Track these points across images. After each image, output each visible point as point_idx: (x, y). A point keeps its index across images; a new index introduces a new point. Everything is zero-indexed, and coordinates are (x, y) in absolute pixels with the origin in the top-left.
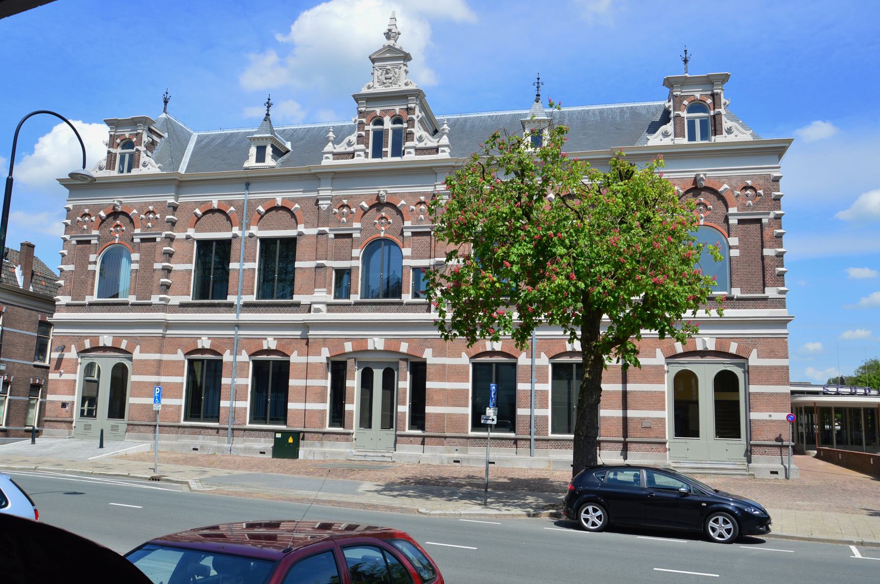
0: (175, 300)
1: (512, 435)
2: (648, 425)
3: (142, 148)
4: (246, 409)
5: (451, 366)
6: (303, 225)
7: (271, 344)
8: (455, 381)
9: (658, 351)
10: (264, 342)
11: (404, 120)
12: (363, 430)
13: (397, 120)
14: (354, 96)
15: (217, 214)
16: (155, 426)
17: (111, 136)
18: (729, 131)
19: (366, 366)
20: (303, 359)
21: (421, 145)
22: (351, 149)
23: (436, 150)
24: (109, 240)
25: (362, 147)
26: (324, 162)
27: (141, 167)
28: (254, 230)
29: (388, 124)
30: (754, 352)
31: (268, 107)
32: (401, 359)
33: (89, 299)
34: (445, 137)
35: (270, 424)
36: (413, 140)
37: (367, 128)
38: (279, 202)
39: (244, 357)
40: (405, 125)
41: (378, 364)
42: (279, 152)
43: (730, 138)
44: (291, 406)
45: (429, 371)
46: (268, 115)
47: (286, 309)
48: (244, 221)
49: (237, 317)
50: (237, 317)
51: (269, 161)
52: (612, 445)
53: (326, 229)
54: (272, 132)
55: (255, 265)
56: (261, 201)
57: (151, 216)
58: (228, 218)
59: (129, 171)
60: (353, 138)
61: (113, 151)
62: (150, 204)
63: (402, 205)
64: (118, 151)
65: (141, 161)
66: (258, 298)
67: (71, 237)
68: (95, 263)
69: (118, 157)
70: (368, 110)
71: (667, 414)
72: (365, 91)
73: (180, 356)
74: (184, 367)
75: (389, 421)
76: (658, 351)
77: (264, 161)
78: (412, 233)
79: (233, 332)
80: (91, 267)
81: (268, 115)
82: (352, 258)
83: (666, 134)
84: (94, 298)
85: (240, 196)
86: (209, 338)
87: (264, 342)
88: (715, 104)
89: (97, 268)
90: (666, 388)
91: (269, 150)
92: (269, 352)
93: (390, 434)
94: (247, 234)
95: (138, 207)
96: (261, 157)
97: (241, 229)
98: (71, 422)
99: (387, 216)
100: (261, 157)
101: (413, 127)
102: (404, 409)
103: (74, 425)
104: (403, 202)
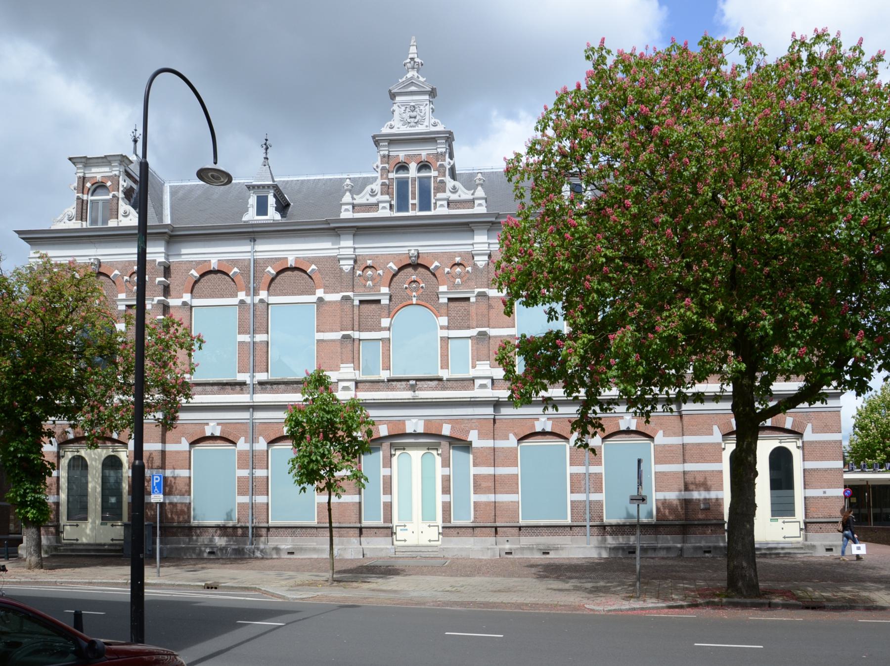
9: (715, 428)
10: (621, 422)
13: (424, 166)
15: (296, 272)
21: (454, 197)
22: (373, 200)
23: (471, 203)
25: (387, 198)
29: (413, 172)
30: (809, 427)
31: (267, 149)
34: (480, 188)
36: (445, 191)
40: (434, 173)
42: (283, 207)
49: (252, 398)
53: (350, 294)
54: (274, 181)
56: (393, 257)
61: (85, 197)
63: (116, 275)
65: (121, 212)
76: (715, 428)
77: (266, 214)
82: (382, 329)
86: (218, 424)
87: (536, 423)
91: (272, 201)
94: (257, 299)
95: (120, 267)
96: (262, 209)
100: (262, 209)
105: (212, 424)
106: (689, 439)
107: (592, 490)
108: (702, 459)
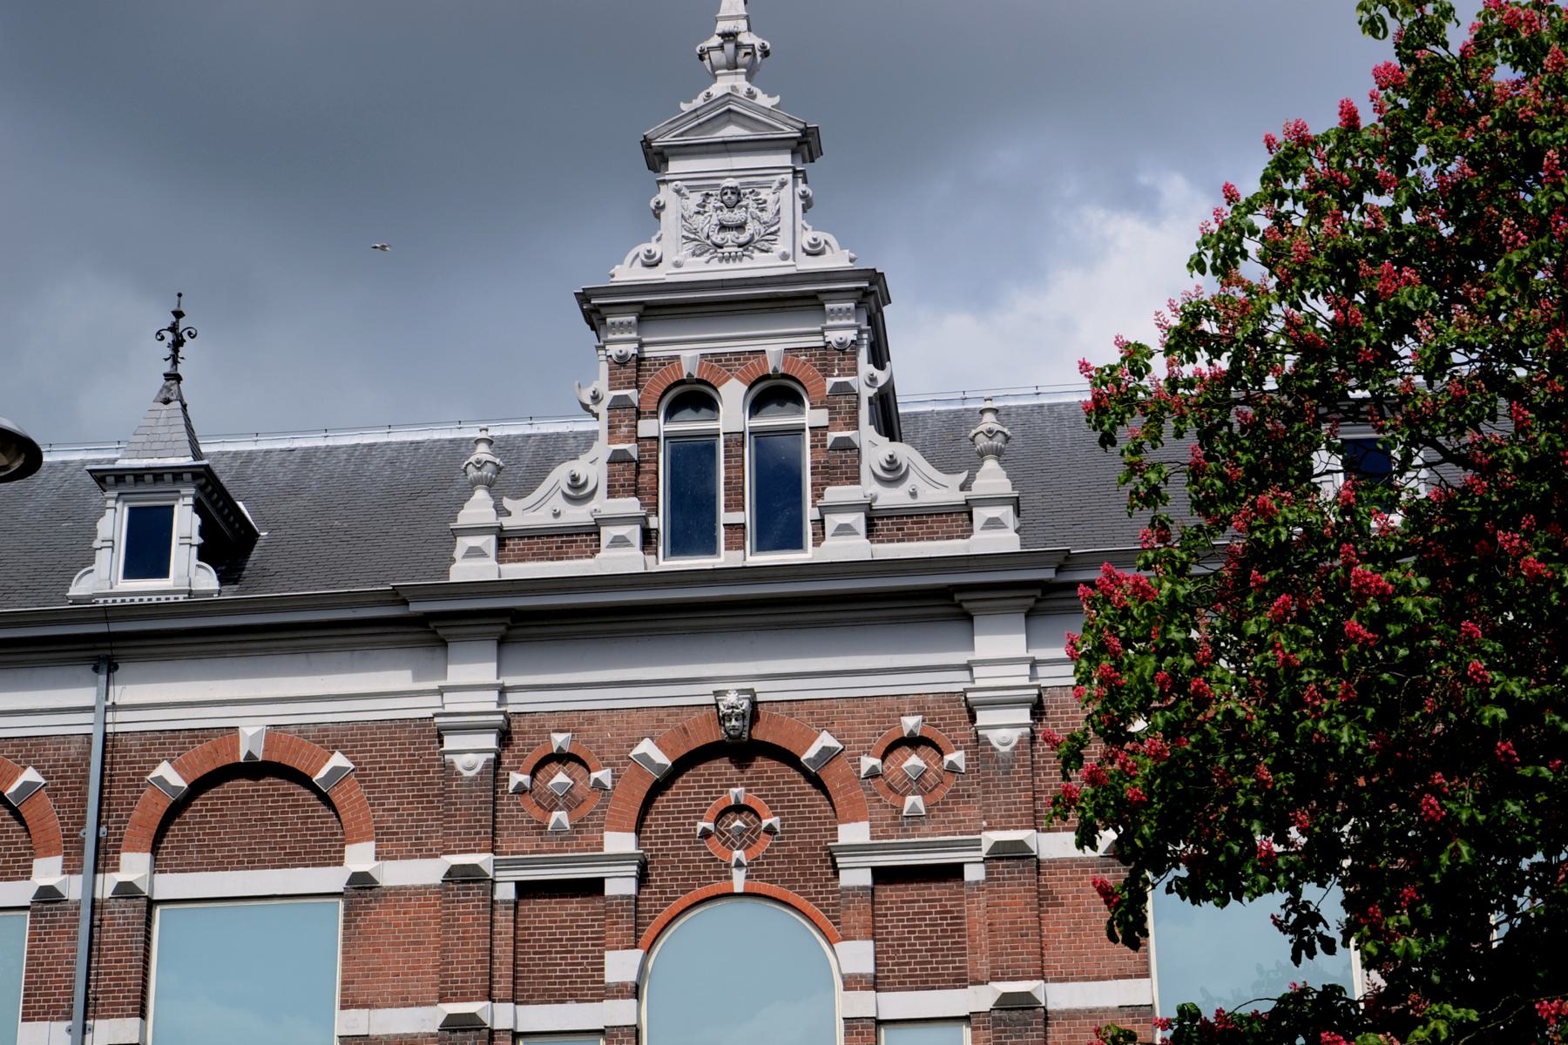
6: (369, 847)
13: (774, 392)
21: (890, 498)
22: (578, 515)
23: (960, 516)
24: (699, 877)
26: (463, 570)
29: (732, 410)
36: (855, 479)
37: (647, 428)
38: (251, 741)
40: (812, 417)
42: (227, 543)
53: (483, 860)
54: (197, 454)
57: (914, 761)
60: (593, 467)
63: (336, 771)
72: (628, 272)
77: (162, 571)
81: (174, 377)
82: (604, 992)
91: (186, 523)
94: (107, 885)
96: (147, 553)
99: (757, 803)
100: (147, 553)
104: (826, 740)
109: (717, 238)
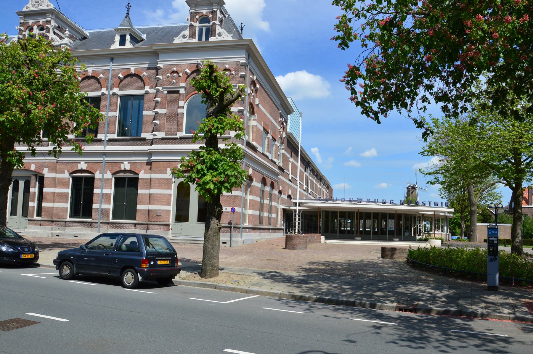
0: (160, 135)
1: (89, 220)
2: (160, 214)
3: (217, 22)
4: (67, 208)
5: (59, 179)
7: (126, 166)
8: (61, 188)
9: (169, 170)
10: (122, 165)
11: (45, 28)
12: (13, 217)
14: (17, 13)
16: (231, 227)
17: (191, 13)
18: (220, 35)
19: (26, 179)
20: (148, 176)
27: (217, 36)
28: (116, 90)
29: (36, 31)
32: (32, 175)
33: (179, 134)
35: (82, 218)
37: (24, 33)
38: (133, 71)
39: (108, 175)
40: (44, 31)
41: (22, 178)
42: (135, 40)
43: (220, 39)
44: (139, 207)
45: (46, 181)
46: (128, 14)
47: (115, 143)
48: (110, 84)
49: (105, 148)
50: (105, 148)
51: (128, 45)
52: (142, 226)
55: (117, 114)
58: (142, 80)
59: (207, 38)
61: (194, 24)
62: (227, 63)
63: (144, 75)
64: (197, 24)
65: (217, 31)
66: (118, 135)
67: (163, 88)
68: (183, 107)
69: (197, 29)
70: (25, 22)
71: (172, 208)
72: (25, 9)
73: (66, 175)
74: (69, 182)
75: (25, 213)
77: (124, 45)
78: (168, 91)
79: (102, 159)
80: (180, 111)
81: (128, 14)
83: (184, 37)
84: (183, 134)
85: (111, 67)
87: (79, 165)
88: (214, 18)
89: (185, 111)
90: (173, 192)
91: (128, 38)
92: (82, 171)
93: (25, 219)
96: (122, 42)
97: (107, 89)
98: (169, 225)
101: (49, 33)
102: (33, 205)
103: (170, 227)
105: (82, 163)
106: (154, 176)
107: (104, 203)
108: (160, 187)
109: (35, 4)
